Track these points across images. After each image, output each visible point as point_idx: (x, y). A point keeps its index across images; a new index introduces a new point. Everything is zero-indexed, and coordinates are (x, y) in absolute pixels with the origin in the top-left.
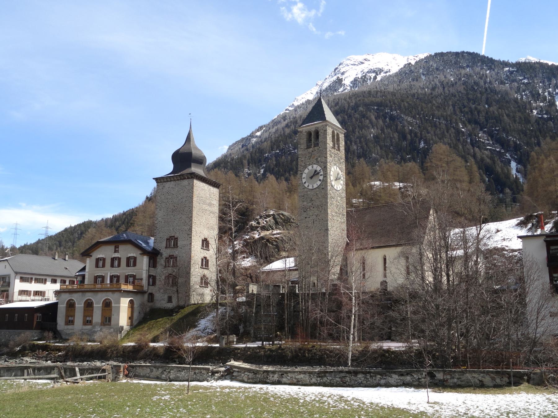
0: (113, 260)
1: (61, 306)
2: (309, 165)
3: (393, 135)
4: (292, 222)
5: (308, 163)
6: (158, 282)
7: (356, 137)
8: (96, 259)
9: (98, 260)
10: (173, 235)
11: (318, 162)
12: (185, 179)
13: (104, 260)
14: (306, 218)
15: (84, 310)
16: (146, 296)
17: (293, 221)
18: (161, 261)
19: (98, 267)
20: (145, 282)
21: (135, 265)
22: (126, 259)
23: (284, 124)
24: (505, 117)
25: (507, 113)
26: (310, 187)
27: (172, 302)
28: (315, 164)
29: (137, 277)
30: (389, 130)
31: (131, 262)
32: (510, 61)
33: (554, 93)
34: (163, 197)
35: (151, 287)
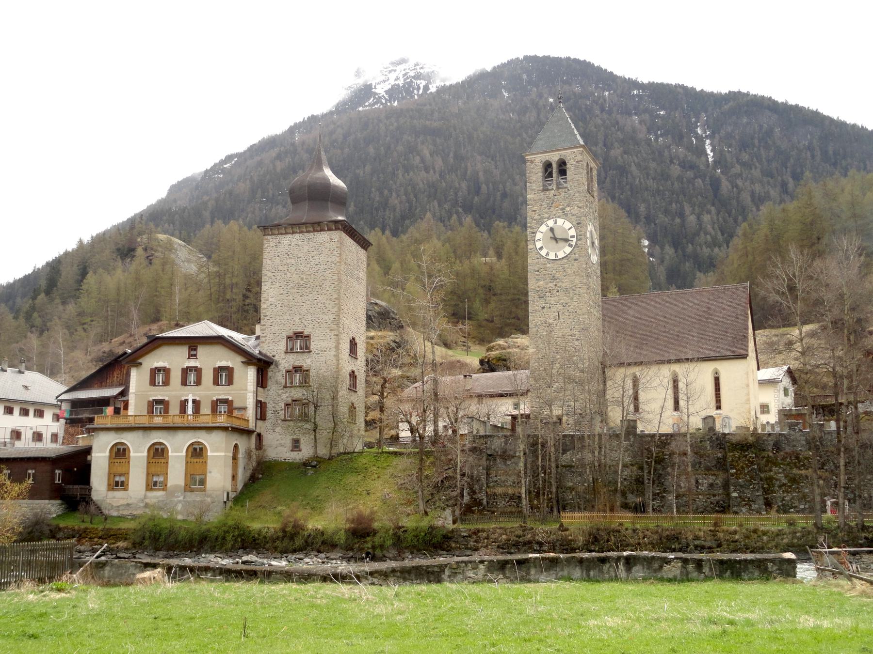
0: (186, 371)
1: (97, 455)
2: (549, 218)
3: (459, 184)
4: (393, 318)
5: (546, 215)
6: (269, 414)
7: (398, 184)
8: (151, 369)
9: (155, 372)
10: (300, 330)
11: (566, 215)
12: (322, 230)
13: (166, 371)
14: (543, 308)
15: (149, 463)
16: (253, 437)
17: (393, 316)
18: (277, 376)
19: (186, 385)
20: (251, 413)
21: (230, 382)
22: (212, 371)
23: (273, 153)
24: (633, 168)
25: (636, 161)
26: (552, 256)
27: (300, 450)
28: (559, 217)
29: (236, 405)
30: (454, 176)
31: (224, 375)
32: (639, 80)
33: (704, 136)
34: (277, 261)
35: (260, 423)
